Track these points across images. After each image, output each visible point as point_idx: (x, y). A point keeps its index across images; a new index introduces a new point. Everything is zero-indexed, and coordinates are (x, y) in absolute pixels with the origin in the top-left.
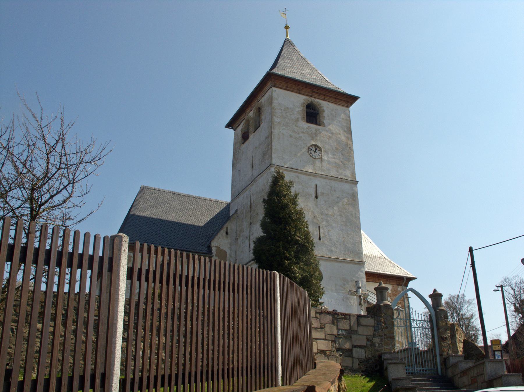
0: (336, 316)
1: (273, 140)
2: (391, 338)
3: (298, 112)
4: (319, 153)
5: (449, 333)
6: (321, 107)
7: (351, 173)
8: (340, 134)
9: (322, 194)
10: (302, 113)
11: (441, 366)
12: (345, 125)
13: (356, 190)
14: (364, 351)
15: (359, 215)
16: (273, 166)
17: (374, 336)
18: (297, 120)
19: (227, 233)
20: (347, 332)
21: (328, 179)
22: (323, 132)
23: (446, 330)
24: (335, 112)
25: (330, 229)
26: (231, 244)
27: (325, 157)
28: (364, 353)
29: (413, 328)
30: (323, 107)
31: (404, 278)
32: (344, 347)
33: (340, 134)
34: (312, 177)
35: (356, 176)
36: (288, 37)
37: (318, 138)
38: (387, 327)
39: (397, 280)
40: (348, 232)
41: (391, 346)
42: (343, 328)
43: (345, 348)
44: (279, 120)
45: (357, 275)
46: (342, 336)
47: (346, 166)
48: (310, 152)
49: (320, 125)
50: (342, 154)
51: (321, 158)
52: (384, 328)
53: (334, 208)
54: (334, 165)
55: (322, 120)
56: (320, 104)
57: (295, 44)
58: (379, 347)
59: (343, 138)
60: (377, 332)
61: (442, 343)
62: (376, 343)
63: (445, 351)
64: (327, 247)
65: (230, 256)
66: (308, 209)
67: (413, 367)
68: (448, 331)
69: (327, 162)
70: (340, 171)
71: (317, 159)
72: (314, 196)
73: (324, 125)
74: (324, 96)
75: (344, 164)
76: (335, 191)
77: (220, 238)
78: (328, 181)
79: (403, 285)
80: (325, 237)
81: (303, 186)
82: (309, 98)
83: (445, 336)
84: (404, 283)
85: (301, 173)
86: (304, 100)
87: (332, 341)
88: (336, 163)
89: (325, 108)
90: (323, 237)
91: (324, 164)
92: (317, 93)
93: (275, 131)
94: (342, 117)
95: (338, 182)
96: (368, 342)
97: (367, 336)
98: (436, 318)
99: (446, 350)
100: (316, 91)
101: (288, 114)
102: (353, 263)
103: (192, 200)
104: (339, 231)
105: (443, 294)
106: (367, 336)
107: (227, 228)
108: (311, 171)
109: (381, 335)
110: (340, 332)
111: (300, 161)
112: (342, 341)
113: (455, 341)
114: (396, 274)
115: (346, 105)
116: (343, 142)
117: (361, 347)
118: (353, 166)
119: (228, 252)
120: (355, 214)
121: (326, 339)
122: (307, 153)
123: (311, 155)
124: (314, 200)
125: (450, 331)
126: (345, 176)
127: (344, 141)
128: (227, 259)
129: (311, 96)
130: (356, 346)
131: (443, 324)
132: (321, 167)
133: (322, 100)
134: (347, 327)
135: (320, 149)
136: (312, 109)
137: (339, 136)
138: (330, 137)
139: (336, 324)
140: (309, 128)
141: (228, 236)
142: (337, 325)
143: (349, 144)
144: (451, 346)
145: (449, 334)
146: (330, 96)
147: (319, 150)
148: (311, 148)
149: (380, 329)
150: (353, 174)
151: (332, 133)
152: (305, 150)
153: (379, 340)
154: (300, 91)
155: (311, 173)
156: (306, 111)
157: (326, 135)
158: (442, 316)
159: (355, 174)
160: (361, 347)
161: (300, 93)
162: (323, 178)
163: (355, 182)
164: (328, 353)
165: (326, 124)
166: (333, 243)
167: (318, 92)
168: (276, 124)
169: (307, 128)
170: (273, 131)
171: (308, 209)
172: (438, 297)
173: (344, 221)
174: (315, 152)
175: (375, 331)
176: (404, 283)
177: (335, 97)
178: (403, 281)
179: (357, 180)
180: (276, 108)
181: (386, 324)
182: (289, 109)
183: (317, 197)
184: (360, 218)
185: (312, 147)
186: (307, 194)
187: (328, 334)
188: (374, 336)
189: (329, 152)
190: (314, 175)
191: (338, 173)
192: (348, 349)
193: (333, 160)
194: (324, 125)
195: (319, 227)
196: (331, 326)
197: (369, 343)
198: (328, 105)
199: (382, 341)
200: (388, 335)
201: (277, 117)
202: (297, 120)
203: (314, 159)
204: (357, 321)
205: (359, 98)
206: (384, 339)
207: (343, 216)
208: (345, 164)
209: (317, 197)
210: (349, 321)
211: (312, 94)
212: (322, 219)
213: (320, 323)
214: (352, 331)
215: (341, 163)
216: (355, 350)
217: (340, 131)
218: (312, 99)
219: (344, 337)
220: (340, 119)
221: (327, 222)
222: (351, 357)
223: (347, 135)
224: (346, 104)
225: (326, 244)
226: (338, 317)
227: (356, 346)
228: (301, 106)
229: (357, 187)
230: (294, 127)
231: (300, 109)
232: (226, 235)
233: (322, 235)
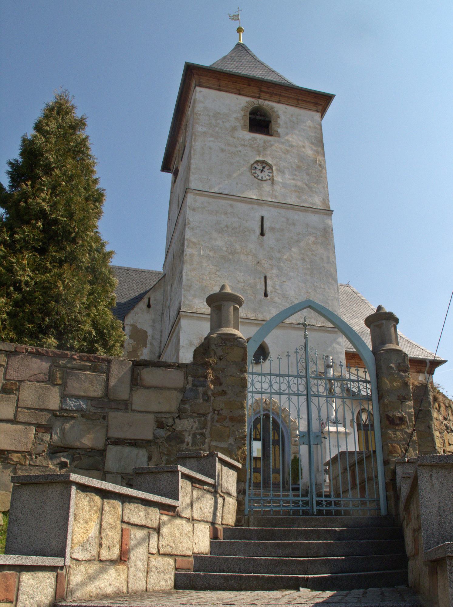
0: (62, 362)
1: (192, 156)
2: (232, 419)
3: (237, 118)
4: (269, 172)
5: (410, 408)
6: (274, 112)
7: (322, 199)
8: (304, 147)
9: (273, 229)
10: (243, 119)
11: (386, 491)
12: (313, 134)
13: (330, 223)
14: (146, 455)
15: (335, 258)
16: (191, 191)
17: (181, 414)
18: (234, 129)
19: (149, 306)
20: (94, 402)
21: (281, 207)
22: (277, 144)
23: (403, 399)
24: (297, 119)
25: (285, 280)
26: (154, 321)
27: (278, 178)
28: (145, 459)
29: (313, 398)
30: (277, 111)
31: (427, 361)
32: (78, 444)
33: (304, 147)
34: (256, 206)
35: (330, 204)
36: (241, 42)
37: (268, 152)
38: (224, 393)
39: (416, 366)
40: (315, 284)
41: (231, 441)
42: (82, 394)
43: (81, 447)
44: (205, 129)
45: (330, 349)
46: (75, 415)
47: (314, 189)
48: (253, 171)
49: (271, 135)
50: (308, 174)
51: (272, 180)
52: (213, 394)
53: (293, 249)
54: (293, 189)
55: (275, 129)
56: (272, 108)
57: (249, 48)
58: (194, 443)
59: (309, 152)
60: (191, 406)
61: (390, 432)
62: (186, 434)
63: (397, 453)
64: (278, 307)
65: (153, 338)
66: (246, 251)
67: (309, 497)
68: (410, 403)
69: (281, 186)
70: (304, 197)
71: (265, 181)
72: (258, 231)
73: (278, 135)
74: (279, 97)
75: (310, 188)
76: (294, 224)
77: (137, 313)
78: (282, 211)
79: (426, 372)
80: (275, 292)
81: (239, 218)
82: (255, 100)
83: (399, 415)
84: (427, 369)
85: (237, 201)
86: (247, 102)
87: (39, 426)
88: (296, 186)
89: (280, 113)
90: (271, 292)
91: (277, 187)
92: (267, 93)
93: (196, 144)
94: (308, 125)
95: (299, 212)
96: (158, 430)
97: (159, 416)
98: (377, 370)
99: (399, 449)
100: (267, 90)
101: (220, 121)
102: (324, 330)
103: (120, 272)
104: (300, 283)
105: (397, 315)
106: (159, 416)
107: (149, 299)
108: (254, 197)
109: (202, 412)
110: (71, 404)
111: (237, 184)
112: (72, 427)
113: (429, 427)
114: (414, 356)
115: (315, 108)
116: (310, 157)
117: (134, 443)
118: (326, 189)
119: (150, 332)
120: (328, 257)
121: (18, 419)
122: (249, 173)
123: (256, 175)
124: (258, 239)
125: (415, 401)
126: (312, 204)
127: (311, 156)
128: (147, 342)
129: (259, 98)
130: (118, 442)
131: (395, 384)
132: (271, 192)
133: (276, 102)
134: (97, 391)
135: (271, 167)
136: (261, 115)
137: (303, 149)
138: (287, 151)
139: (59, 382)
140: (255, 139)
141: (150, 309)
142: (64, 385)
143: (319, 161)
144: (415, 438)
145: (412, 410)
146: (288, 97)
147: (269, 168)
148: (255, 165)
149: (201, 396)
150: (326, 200)
151: (292, 146)
152: (245, 168)
153: (196, 425)
154: (239, 90)
155: (253, 200)
156: (250, 118)
157: (281, 149)
158: (392, 365)
159: (329, 201)
160: (134, 443)
161: (240, 94)
162: (274, 206)
163: (329, 212)
164: (15, 457)
165: (281, 135)
166: (289, 301)
167: (268, 91)
168: (199, 134)
169: (249, 139)
170: (193, 143)
171: (246, 251)
172: (384, 322)
173: (308, 269)
174: (262, 171)
175: (183, 401)
176: (427, 369)
177: (296, 97)
178: (426, 366)
179: (331, 209)
180: (200, 114)
181: (221, 384)
182: (221, 115)
183: (262, 234)
184: (335, 264)
185: (257, 164)
186: (246, 230)
187: (28, 409)
188: (181, 414)
189: (286, 171)
190: (260, 202)
191: (299, 200)
192: (93, 449)
193: (293, 181)
194: (278, 135)
195: (265, 277)
196: (40, 387)
197: (162, 433)
198: (286, 108)
199: (204, 427)
200: (225, 412)
201: (202, 125)
202: (234, 129)
203: (260, 182)
204: (133, 375)
205: (334, 96)
206: (213, 422)
207: (308, 260)
208: (311, 188)
209: (262, 234)
210: (104, 376)
211: (259, 94)
212: (271, 265)
213: (5, 378)
214: (110, 400)
215: (305, 186)
216: (112, 452)
217: (304, 143)
218: (260, 101)
219: (83, 416)
220: (306, 128)
221: (278, 269)
222: (97, 470)
223: (316, 149)
224: (315, 107)
225: (276, 303)
226: (69, 365)
227: (118, 442)
228: (242, 110)
229: (331, 219)
230: (230, 139)
231: (239, 115)
232: (147, 308)
233: (269, 289)
